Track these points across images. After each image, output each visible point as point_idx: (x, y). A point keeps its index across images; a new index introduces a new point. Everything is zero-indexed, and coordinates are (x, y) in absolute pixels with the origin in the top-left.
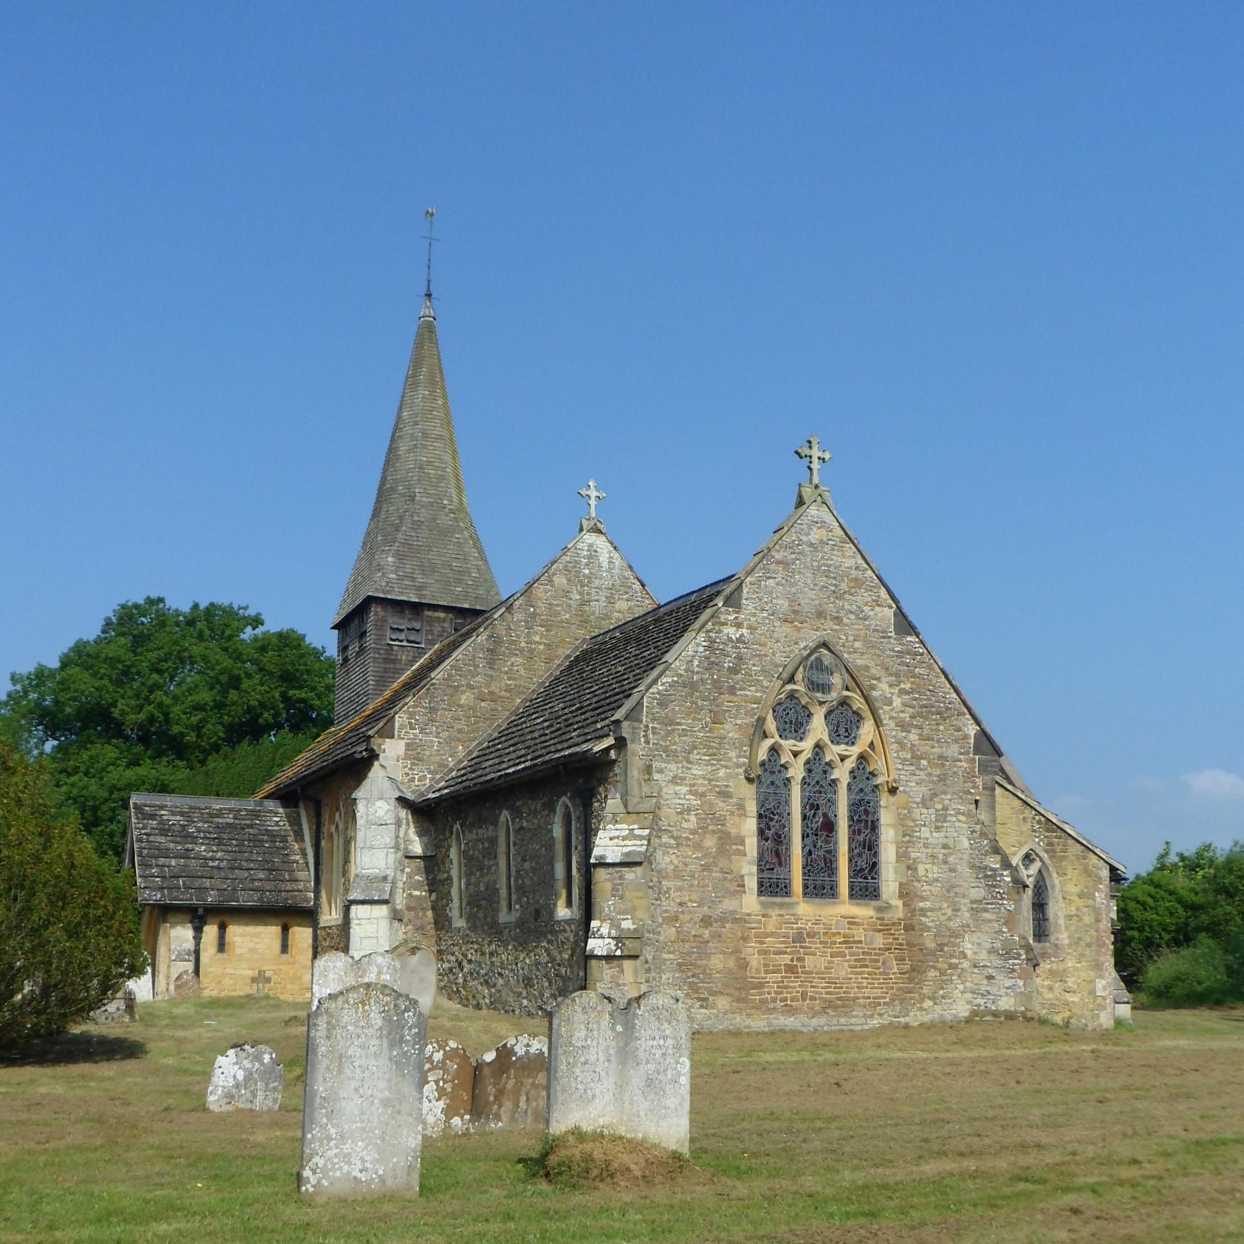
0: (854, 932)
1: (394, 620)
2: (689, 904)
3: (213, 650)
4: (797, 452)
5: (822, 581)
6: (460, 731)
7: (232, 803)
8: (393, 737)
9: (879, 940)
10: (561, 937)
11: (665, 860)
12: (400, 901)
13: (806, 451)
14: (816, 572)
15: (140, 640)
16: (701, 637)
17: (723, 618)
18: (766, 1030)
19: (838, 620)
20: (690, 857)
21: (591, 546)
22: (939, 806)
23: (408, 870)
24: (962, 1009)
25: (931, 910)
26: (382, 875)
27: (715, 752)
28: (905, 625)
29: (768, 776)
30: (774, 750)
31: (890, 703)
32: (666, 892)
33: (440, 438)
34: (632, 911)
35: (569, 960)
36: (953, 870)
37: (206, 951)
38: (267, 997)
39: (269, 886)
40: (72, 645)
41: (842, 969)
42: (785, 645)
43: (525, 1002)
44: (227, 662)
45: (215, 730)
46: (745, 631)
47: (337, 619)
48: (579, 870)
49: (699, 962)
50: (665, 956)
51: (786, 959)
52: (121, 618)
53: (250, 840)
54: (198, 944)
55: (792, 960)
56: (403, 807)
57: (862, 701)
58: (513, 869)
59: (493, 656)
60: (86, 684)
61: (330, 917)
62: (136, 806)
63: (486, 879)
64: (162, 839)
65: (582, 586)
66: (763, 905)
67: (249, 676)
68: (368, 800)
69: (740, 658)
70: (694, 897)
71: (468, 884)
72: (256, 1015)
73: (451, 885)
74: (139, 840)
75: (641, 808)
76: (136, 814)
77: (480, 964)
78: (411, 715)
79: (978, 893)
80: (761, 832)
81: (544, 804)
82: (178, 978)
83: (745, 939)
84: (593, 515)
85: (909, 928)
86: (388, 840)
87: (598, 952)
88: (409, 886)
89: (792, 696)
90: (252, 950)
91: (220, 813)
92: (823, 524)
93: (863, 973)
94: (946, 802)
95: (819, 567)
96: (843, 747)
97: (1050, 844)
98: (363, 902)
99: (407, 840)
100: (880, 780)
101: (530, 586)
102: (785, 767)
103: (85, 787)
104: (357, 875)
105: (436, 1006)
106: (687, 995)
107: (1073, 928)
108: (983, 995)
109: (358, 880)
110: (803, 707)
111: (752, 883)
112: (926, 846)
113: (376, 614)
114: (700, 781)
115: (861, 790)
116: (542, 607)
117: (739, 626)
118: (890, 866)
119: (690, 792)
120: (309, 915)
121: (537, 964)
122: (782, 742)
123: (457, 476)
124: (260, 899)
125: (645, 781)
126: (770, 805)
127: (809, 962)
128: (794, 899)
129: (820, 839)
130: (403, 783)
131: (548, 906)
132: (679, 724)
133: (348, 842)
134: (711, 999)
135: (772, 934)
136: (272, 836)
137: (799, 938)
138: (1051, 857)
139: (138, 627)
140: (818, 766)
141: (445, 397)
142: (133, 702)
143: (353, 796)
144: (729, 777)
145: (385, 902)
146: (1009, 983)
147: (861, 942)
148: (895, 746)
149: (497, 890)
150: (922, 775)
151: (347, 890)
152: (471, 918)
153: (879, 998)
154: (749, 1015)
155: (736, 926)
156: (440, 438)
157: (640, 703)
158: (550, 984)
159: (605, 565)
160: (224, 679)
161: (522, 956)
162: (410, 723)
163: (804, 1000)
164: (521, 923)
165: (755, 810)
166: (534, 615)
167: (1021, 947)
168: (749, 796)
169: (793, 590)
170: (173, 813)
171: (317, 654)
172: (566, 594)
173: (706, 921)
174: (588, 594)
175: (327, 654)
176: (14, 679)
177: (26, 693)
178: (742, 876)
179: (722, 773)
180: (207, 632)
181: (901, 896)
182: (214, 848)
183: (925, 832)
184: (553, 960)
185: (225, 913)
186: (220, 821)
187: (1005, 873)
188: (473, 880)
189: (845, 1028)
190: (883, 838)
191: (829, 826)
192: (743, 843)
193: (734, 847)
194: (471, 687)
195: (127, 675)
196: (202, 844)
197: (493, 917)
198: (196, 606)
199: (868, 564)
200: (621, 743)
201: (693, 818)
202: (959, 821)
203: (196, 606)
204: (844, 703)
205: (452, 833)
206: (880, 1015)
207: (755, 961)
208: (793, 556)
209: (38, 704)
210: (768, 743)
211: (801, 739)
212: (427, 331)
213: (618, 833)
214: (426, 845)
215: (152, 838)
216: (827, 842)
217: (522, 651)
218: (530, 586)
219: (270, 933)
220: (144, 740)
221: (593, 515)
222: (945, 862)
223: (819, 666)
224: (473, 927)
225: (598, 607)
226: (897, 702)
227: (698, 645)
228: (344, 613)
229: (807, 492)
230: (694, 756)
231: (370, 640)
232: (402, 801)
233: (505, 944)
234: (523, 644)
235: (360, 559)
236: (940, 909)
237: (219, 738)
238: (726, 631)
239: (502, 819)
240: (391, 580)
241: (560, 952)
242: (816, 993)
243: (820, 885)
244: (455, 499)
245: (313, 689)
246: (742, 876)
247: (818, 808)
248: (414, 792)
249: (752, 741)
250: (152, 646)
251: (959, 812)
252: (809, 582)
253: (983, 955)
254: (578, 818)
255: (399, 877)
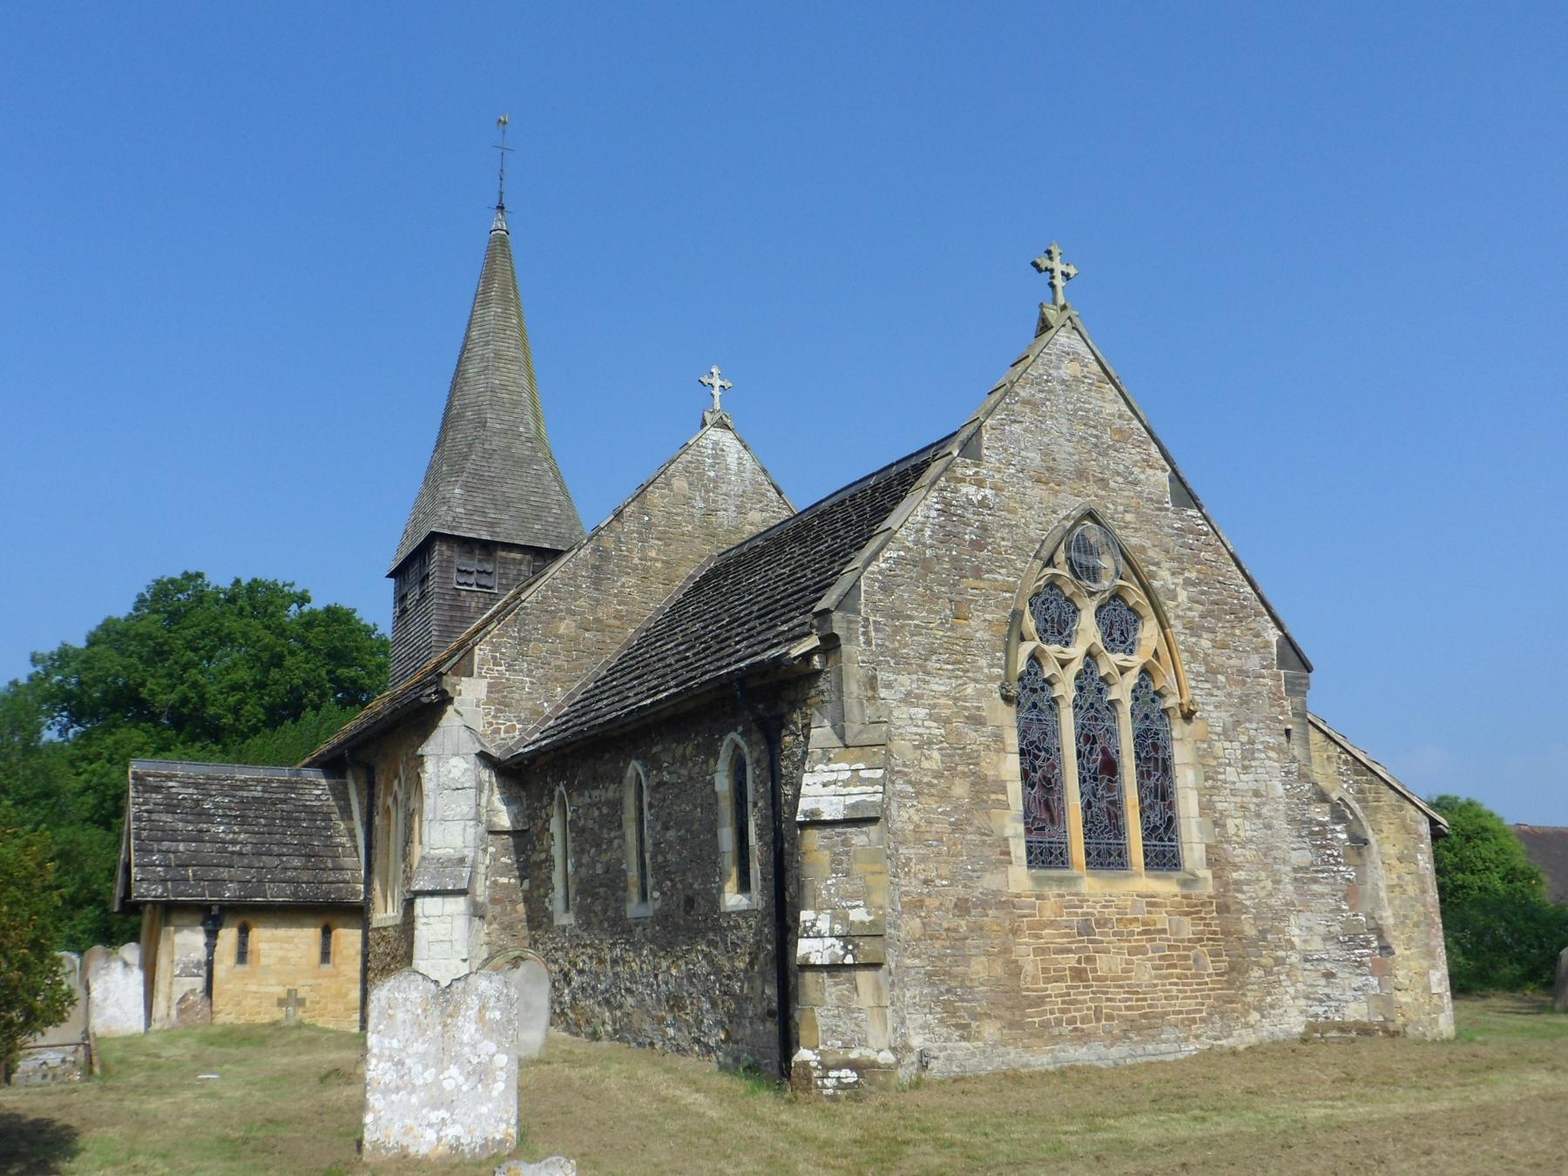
0: (1155, 917)
1: (462, 561)
2: (938, 882)
3: (256, 628)
4: (1035, 264)
5: (1080, 430)
6: (558, 668)
7: (261, 773)
8: (471, 675)
9: (1188, 928)
10: (731, 937)
11: (903, 817)
12: (482, 891)
13: (1045, 263)
14: (1072, 416)
15: (175, 617)
16: (933, 497)
17: (959, 471)
18: (1051, 1068)
19: (1103, 482)
20: (934, 811)
21: (716, 443)
22: (1244, 739)
23: (491, 849)
24: (1293, 1023)
25: (1248, 882)
26: (458, 856)
27: (960, 656)
28: (1184, 495)
29: (1029, 696)
30: (1035, 659)
31: (1174, 598)
32: (905, 865)
33: (514, 360)
34: (865, 894)
35: (746, 971)
36: (1268, 827)
37: (221, 961)
38: (300, 1025)
39: (305, 876)
40: (100, 623)
41: (1144, 973)
42: (1041, 513)
43: (671, 1032)
44: (268, 638)
45: (254, 710)
46: (988, 492)
47: (393, 566)
48: (760, 837)
49: (956, 970)
50: (908, 962)
51: (1071, 960)
52: (155, 594)
53: (282, 819)
54: (211, 953)
55: (1079, 962)
56: (486, 767)
57: (1142, 593)
58: (649, 842)
59: (599, 576)
60: (112, 662)
61: (385, 914)
62: (136, 776)
63: (605, 858)
64: (168, 818)
65: (707, 492)
66: (1037, 880)
67: (292, 653)
68: (439, 757)
69: (984, 528)
70: (944, 871)
71: (578, 865)
72: (279, 1060)
73: (552, 867)
74: (138, 819)
75: (865, 738)
76: (135, 786)
77: (597, 975)
78: (496, 648)
79: (1303, 857)
80: (1025, 775)
81: (698, 746)
82: (183, 999)
83: (1015, 932)
84: (718, 407)
85: (1223, 909)
86: (466, 809)
87: (816, 959)
88: (493, 871)
89: (1052, 584)
90: (282, 960)
91: (244, 786)
92: (1075, 357)
93: (1171, 976)
94: (1252, 732)
95: (1076, 411)
96: (1121, 656)
97: (1361, 791)
98: (432, 894)
99: (492, 811)
100: (1171, 702)
101: (643, 489)
102: (1049, 682)
103: (107, 774)
104: (423, 858)
105: (549, 1042)
106: (941, 1021)
107: (1397, 902)
108: (1321, 1001)
109: (425, 864)
110: (1068, 600)
111: (1019, 849)
112: (1234, 793)
113: (441, 554)
114: (942, 701)
115: (1147, 717)
116: (658, 517)
117: (980, 484)
118: (1193, 821)
119: (931, 717)
120: (358, 913)
121: (691, 976)
122: (1045, 647)
123: (534, 403)
124: (294, 894)
125: (869, 699)
126: (1034, 735)
127: (1102, 962)
128: (1075, 872)
129: (1098, 786)
130: (484, 736)
131: (708, 892)
132: (911, 618)
133: (409, 817)
134: (974, 1024)
135: (1051, 924)
136: (312, 812)
137: (1086, 929)
138: (1364, 808)
139: (174, 602)
140: (1091, 683)
141: (520, 316)
142: (164, 681)
143: (420, 752)
144: (980, 695)
145: (462, 892)
146: (1357, 982)
147: (1164, 931)
148: (1185, 656)
149: (624, 873)
150: (1220, 696)
151: (408, 879)
152: (584, 912)
153: (1195, 1011)
154: (1027, 1047)
155: (1001, 914)
156: (514, 360)
157: (855, 586)
158: (714, 1004)
159: (734, 467)
160: (265, 656)
161: (664, 964)
162: (494, 658)
163: (1098, 1020)
164: (662, 918)
165: (1016, 742)
166: (649, 526)
167: (1371, 930)
168: (1006, 719)
169: (1046, 439)
170: (185, 785)
171: (369, 631)
172: (688, 501)
173: (962, 907)
174: (715, 501)
175: (379, 632)
176: (34, 660)
177: (48, 675)
178: (1006, 839)
179: (970, 689)
180: (248, 609)
181: (1210, 863)
182: (236, 829)
183: (1231, 774)
184: (718, 970)
185: (249, 912)
186: (245, 794)
187: (1338, 828)
188: (585, 859)
189: (1153, 1059)
190: (1179, 783)
191: (1111, 766)
192: (1004, 791)
193: (993, 797)
194: (571, 613)
195: (160, 653)
196: (220, 823)
197: (617, 909)
198: (238, 582)
199: (1133, 410)
200: (830, 644)
201: (936, 755)
202: (1269, 758)
203: (238, 582)
204: (1117, 595)
205: (552, 799)
206: (1197, 1037)
207: (1030, 964)
208: (1042, 395)
209: (60, 685)
210: (1027, 648)
211: (1067, 644)
212: (499, 246)
213: (834, 776)
214: (515, 816)
215: (154, 816)
216: (1110, 789)
217: (635, 568)
218: (643, 489)
219: (306, 938)
220: (178, 722)
221: (718, 407)
222: (1259, 815)
223: (1085, 547)
224: (587, 925)
225: (726, 517)
226: (1183, 596)
227: (929, 508)
228: (402, 557)
229: (1052, 314)
230: (932, 665)
231: (433, 585)
232: (484, 757)
233: (637, 948)
234: (636, 561)
235: (421, 495)
236: (1258, 880)
237: (259, 720)
238: (964, 490)
239: (630, 772)
240: (458, 514)
241: (731, 959)
242: (1113, 1008)
243: (1107, 856)
244: (532, 426)
245: (364, 667)
246: (1006, 839)
247: (1094, 742)
248: (499, 747)
249: (1007, 644)
250: (187, 622)
251: (1268, 747)
252: (1064, 430)
253: (1317, 944)
254: (758, 762)
255: (480, 859)
